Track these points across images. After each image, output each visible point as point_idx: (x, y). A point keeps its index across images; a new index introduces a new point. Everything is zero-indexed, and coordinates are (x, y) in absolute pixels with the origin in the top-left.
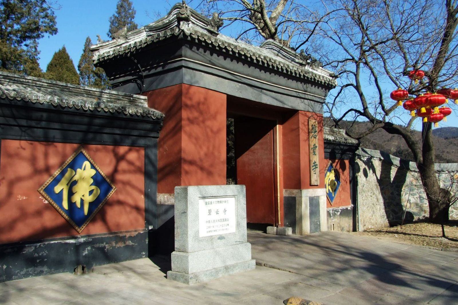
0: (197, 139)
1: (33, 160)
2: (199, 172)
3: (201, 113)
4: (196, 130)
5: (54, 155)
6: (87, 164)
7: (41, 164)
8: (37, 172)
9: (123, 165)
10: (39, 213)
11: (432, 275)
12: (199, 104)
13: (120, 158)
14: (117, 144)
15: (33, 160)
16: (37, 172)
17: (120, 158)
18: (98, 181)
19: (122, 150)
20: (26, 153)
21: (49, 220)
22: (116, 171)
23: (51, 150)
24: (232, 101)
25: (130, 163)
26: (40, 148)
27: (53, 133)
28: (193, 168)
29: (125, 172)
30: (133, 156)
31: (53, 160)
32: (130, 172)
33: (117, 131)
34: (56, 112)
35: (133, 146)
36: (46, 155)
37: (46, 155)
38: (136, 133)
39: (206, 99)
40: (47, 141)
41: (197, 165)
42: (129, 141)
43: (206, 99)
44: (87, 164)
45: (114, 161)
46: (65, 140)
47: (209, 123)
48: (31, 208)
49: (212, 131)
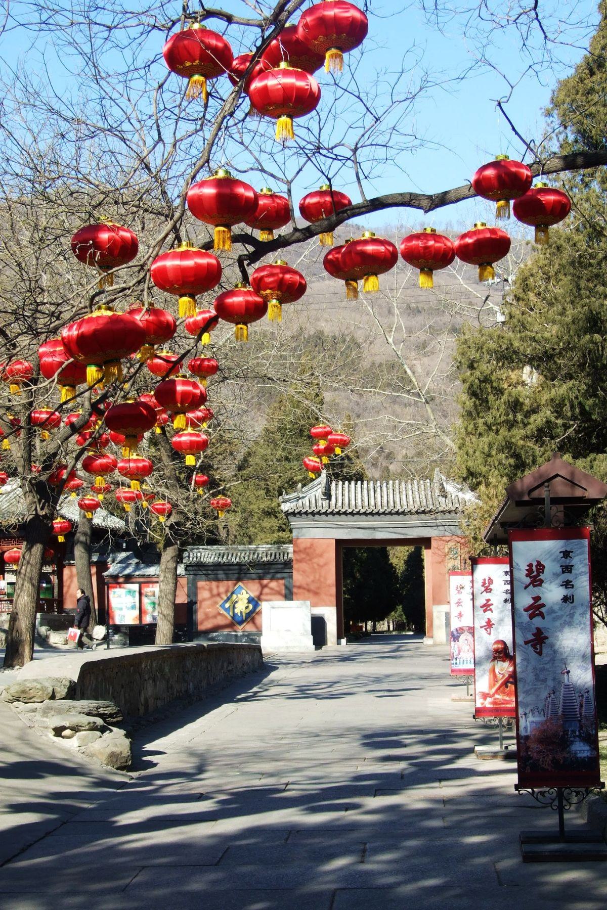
0: (304, 572)
1: (211, 590)
2: (306, 593)
3: (308, 554)
4: (304, 566)
5: (223, 586)
6: (244, 591)
7: (215, 592)
8: (213, 596)
9: (266, 590)
10: (215, 617)
11: (361, 654)
12: (305, 549)
13: (263, 587)
14: (261, 578)
15: (211, 590)
16: (213, 596)
17: (263, 587)
18: (250, 600)
19: (265, 582)
20: (207, 587)
21: (220, 621)
22: (261, 594)
23: (221, 584)
24: (339, 542)
25: (272, 589)
26: (214, 584)
27: (220, 576)
28: (301, 591)
29: (267, 594)
30: (273, 584)
31: (222, 590)
32: (271, 594)
33: (260, 571)
34: (217, 566)
35: (272, 579)
36: (218, 587)
37: (218, 587)
38: (272, 571)
39: (312, 545)
40: (217, 580)
41: (304, 589)
42: (269, 576)
43: (312, 545)
44: (244, 591)
45: (260, 589)
46: (228, 579)
47: (315, 560)
48: (211, 615)
49: (318, 565)
